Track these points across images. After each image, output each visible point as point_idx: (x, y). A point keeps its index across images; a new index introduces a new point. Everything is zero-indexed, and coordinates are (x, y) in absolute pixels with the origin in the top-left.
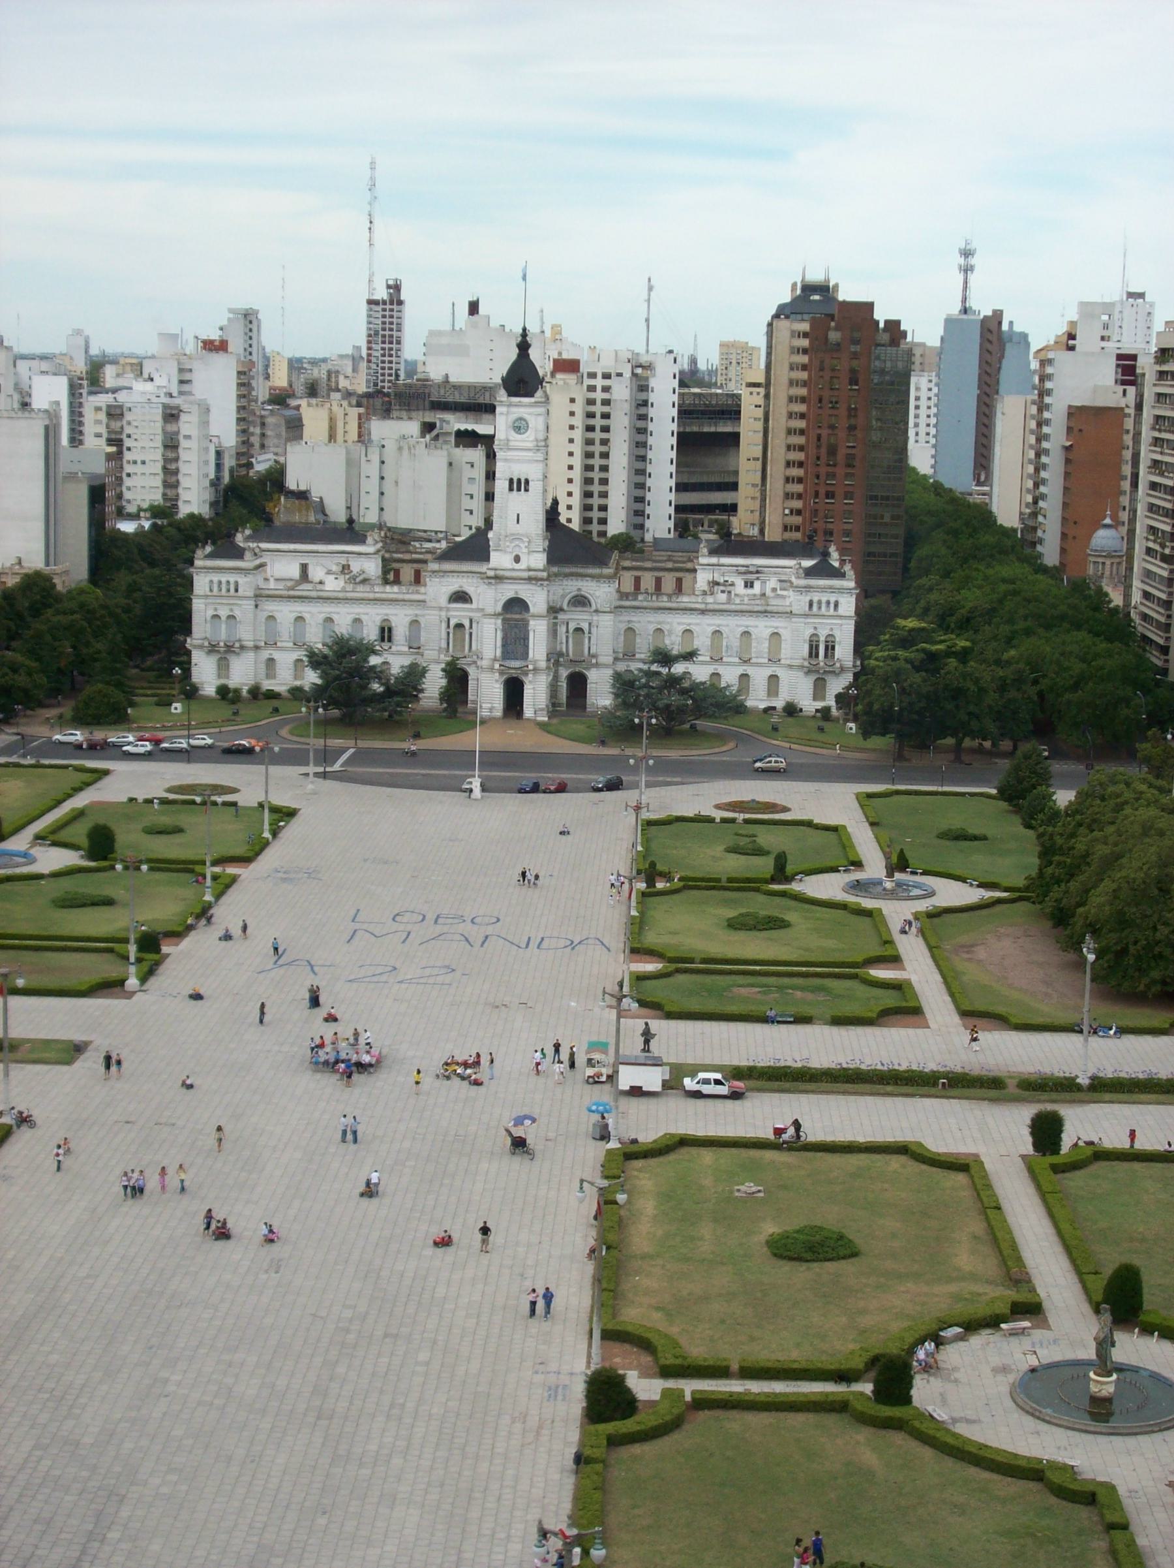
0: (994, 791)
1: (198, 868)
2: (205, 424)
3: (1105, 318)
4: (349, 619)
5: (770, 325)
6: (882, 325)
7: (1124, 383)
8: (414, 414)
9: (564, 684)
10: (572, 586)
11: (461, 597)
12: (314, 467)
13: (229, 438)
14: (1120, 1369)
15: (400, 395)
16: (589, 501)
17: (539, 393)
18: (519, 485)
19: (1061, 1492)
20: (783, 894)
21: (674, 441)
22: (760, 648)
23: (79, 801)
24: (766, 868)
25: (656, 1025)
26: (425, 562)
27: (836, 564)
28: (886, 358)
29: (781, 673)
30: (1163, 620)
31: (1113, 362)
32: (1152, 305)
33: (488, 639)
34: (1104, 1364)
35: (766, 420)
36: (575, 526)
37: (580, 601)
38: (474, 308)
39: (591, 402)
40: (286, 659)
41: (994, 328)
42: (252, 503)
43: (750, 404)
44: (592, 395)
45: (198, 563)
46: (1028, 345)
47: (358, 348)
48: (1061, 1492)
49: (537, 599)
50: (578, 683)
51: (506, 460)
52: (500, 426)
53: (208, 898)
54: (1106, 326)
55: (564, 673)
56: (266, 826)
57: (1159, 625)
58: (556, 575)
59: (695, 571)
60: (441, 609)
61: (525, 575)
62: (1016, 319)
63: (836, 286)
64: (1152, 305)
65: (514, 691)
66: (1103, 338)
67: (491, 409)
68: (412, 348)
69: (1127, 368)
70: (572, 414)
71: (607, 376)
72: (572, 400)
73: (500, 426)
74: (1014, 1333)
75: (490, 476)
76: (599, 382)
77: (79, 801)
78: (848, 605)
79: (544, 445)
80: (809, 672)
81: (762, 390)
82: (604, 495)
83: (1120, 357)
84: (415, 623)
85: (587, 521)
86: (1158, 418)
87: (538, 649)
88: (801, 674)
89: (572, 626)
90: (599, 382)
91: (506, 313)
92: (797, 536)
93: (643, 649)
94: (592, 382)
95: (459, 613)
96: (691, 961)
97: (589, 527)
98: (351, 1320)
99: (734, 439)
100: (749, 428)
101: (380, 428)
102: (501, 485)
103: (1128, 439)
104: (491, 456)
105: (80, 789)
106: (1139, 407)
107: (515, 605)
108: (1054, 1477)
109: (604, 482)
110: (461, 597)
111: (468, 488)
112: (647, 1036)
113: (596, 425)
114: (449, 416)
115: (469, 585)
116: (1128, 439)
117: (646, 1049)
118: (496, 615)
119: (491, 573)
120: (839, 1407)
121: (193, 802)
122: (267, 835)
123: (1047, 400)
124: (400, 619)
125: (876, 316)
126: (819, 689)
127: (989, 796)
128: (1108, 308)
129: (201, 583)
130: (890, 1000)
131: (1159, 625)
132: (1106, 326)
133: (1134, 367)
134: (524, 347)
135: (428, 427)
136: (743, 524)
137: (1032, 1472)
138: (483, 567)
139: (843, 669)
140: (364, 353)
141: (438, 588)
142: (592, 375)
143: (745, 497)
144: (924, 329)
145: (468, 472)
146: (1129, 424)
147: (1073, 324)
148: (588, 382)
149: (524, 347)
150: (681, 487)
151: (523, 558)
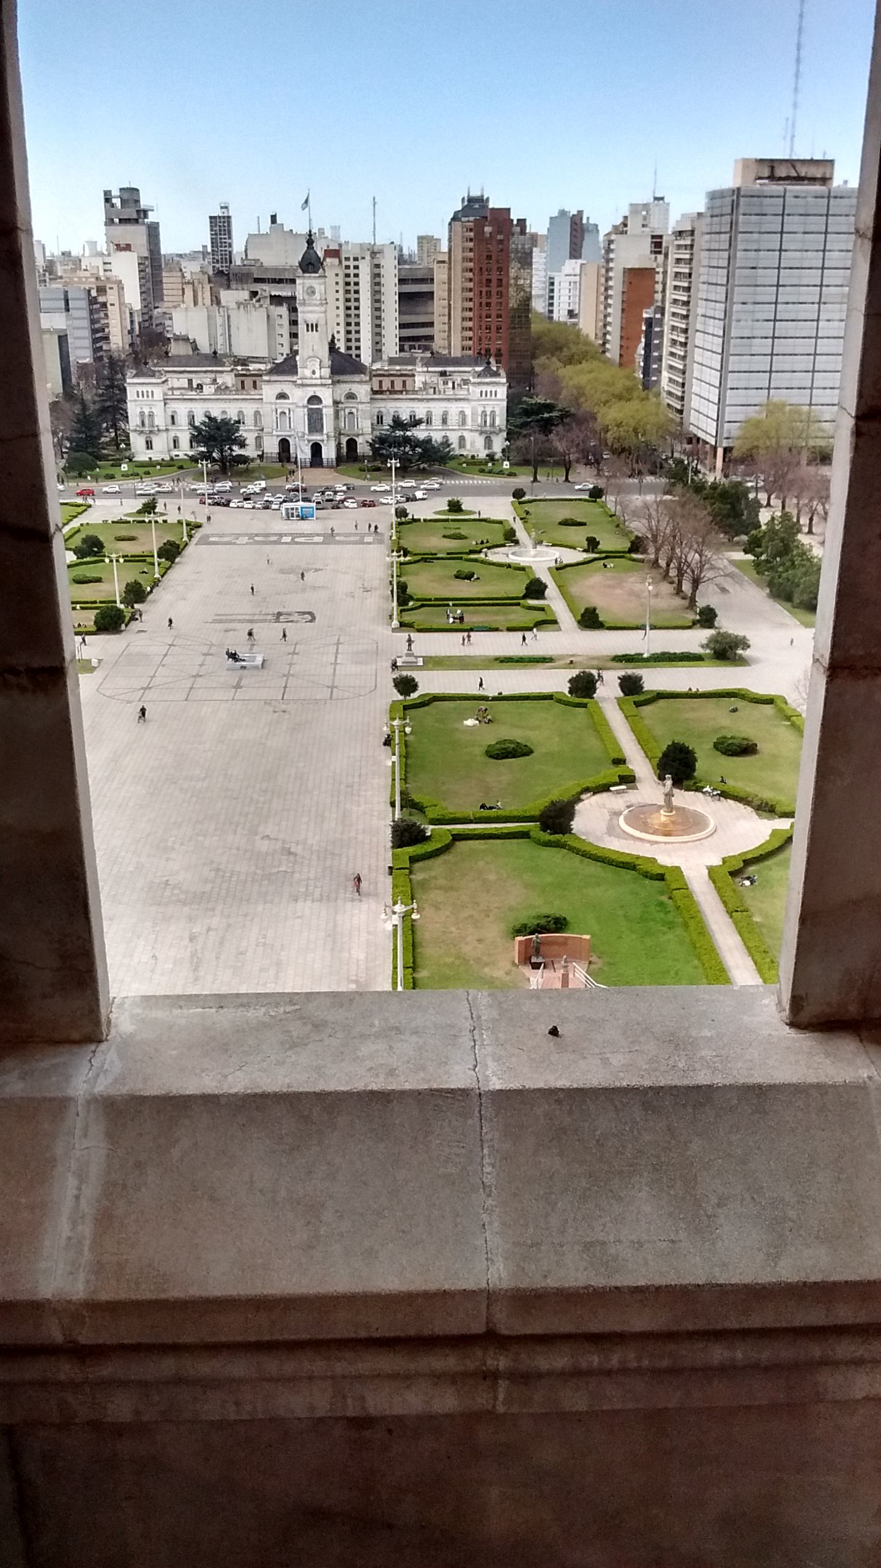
0: (587, 497)
1: (149, 559)
2: (121, 296)
3: (644, 213)
4: (236, 412)
5: (450, 224)
6: (515, 222)
7: (656, 252)
8: (245, 286)
9: (344, 445)
10: (344, 389)
11: (282, 396)
12: (187, 321)
13: (137, 305)
14: (678, 809)
15: (225, 273)
16: (350, 336)
17: (321, 270)
18: (312, 327)
19: (647, 875)
20: (476, 560)
21: (397, 297)
22: (453, 419)
23: (75, 524)
24: (469, 547)
25: (414, 636)
26: (261, 376)
27: (495, 369)
28: (516, 242)
29: (466, 434)
30: (680, 394)
31: (649, 240)
32: (668, 204)
33: (300, 420)
34: (669, 806)
35: (450, 283)
36: (342, 350)
37: (351, 396)
38: (274, 219)
39: (347, 275)
40: (185, 438)
41: (578, 222)
42: (152, 345)
43: (440, 275)
44: (347, 271)
45: (128, 381)
46: (598, 231)
47: (205, 247)
48: (647, 875)
49: (327, 396)
50: (352, 443)
51: (303, 312)
52: (300, 289)
53: (157, 576)
54: (645, 218)
55: (344, 440)
56: (185, 534)
57: (677, 397)
58: (339, 382)
59: (414, 376)
60: (271, 403)
61: (319, 382)
62: (591, 216)
63: (488, 199)
64: (668, 204)
65: (316, 449)
66: (643, 226)
67: (293, 281)
68: (238, 245)
69: (657, 243)
70: (337, 283)
71: (356, 259)
72: (337, 275)
73: (300, 289)
74: (618, 792)
75: (294, 323)
76: (352, 263)
77: (75, 524)
78: (502, 392)
79: (324, 302)
80: (481, 433)
81: (726, 253)
82: (358, 332)
83: (653, 237)
84: (257, 413)
85: (349, 348)
86: (677, 274)
87: (328, 425)
88: (477, 434)
89: (347, 411)
90: (352, 263)
91: (296, 223)
92: (470, 352)
93: (388, 420)
94: (347, 263)
95: (283, 405)
96: (430, 600)
97: (350, 352)
98: (264, 803)
99: (431, 295)
100: (439, 290)
101: (226, 296)
102: (301, 328)
103: (659, 287)
104: (293, 310)
105: (75, 517)
106: (665, 265)
107: (315, 399)
108: (644, 867)
109: (358, 324)
110: (282, 396)
111: (279, 331)
112: (410, 641)
113: (350, 287)
114: (265, 286)
115: (287, 389)
116: (659, 287)
117: (409, 649)
118: (304, 407)
119: (299, 382)
120: (525, 835)
121: (144, 522)
122: (185, 539)
123: (611, 265)
124: (249, 409)
125: (512, 217)
126: (488, 443)
127: (585, 500)
128: (646, 206)
129: (131, 393)
130: (540, 616)
131: (677, 397)
132: (645, 218)
133: (661, 243)
134: (310, 242)
135: (254, 294)
136: (438, 344)
137: (627, 865)
138: (294, 378)
139: (501, 430)
140: (209, 250)
141: (269, 391)
142: (347, 259)
143: (438, 331)
144: (538, 225)
145: (278, 321)
146: (659, 278)
147: (626, 218)
148: (344, 263)
149: (310, 242)
150: (402, 326)
151: (318, 372)
